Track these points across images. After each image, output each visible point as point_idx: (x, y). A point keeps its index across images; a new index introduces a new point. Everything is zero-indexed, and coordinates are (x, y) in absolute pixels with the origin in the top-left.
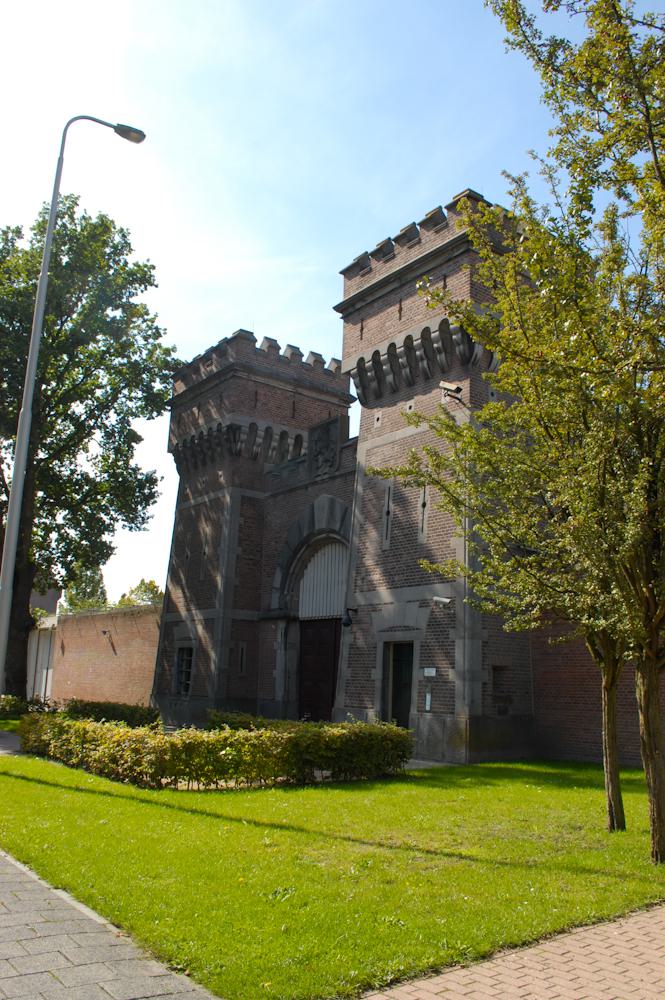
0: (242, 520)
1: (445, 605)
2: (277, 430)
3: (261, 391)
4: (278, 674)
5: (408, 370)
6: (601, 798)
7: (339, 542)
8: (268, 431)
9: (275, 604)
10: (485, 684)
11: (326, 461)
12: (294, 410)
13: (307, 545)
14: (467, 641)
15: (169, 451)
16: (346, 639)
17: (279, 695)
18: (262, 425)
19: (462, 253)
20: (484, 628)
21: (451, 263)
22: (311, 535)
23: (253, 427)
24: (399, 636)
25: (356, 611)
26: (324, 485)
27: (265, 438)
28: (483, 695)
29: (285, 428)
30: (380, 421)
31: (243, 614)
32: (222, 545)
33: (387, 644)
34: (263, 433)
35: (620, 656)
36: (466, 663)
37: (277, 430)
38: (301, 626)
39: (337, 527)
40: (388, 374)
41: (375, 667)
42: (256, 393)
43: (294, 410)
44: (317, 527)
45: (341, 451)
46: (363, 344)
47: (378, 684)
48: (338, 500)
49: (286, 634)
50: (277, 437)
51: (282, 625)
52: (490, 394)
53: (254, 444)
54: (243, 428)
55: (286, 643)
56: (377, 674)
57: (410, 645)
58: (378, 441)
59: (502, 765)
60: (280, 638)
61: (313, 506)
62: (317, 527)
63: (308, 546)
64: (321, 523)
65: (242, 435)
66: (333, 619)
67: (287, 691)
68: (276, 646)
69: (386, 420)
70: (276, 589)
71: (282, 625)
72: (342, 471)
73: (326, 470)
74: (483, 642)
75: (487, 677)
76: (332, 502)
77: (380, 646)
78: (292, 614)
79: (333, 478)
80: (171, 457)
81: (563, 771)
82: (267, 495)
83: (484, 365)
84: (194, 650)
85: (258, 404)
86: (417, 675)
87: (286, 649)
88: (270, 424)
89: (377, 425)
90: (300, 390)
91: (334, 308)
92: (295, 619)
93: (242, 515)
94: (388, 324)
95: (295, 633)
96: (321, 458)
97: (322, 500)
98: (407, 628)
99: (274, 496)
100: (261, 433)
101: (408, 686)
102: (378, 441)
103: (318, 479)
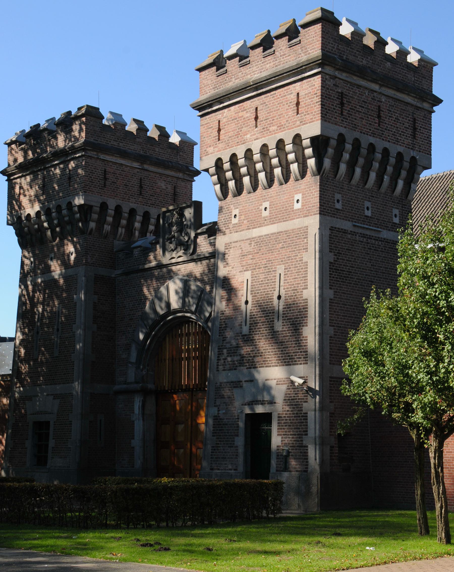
4: (137, 442)
6: (418, 167)
10: (332, 447)
14: (317, 412)
17: (138, 463)
18: (112, 204)
20: (331, 402)
27: (114, 217)
28: (331, 456)
30: (237, 217)
35: (49, 167)
36: (317, 431)
41: (237, 436)
42: (105, 171)
46: (221, 145)
49: (143, 406)
50: (126, 215)
52: (336, 201)
53: (104, 223)
54: (94, 208)
55: (143, 414)
57: (48, 423)
65: (105, 226)
69: (243, 217)
74: (330, 413)
80: (11, 230)
82: (119, 272)
84: (52, 423)
85: (108, 183)
87: (143, 420)
88: (120, 202)
89: (235, 221)
90: (146, 166)
91: (191, 105)
94: (244, 129)
100: (111, 212)
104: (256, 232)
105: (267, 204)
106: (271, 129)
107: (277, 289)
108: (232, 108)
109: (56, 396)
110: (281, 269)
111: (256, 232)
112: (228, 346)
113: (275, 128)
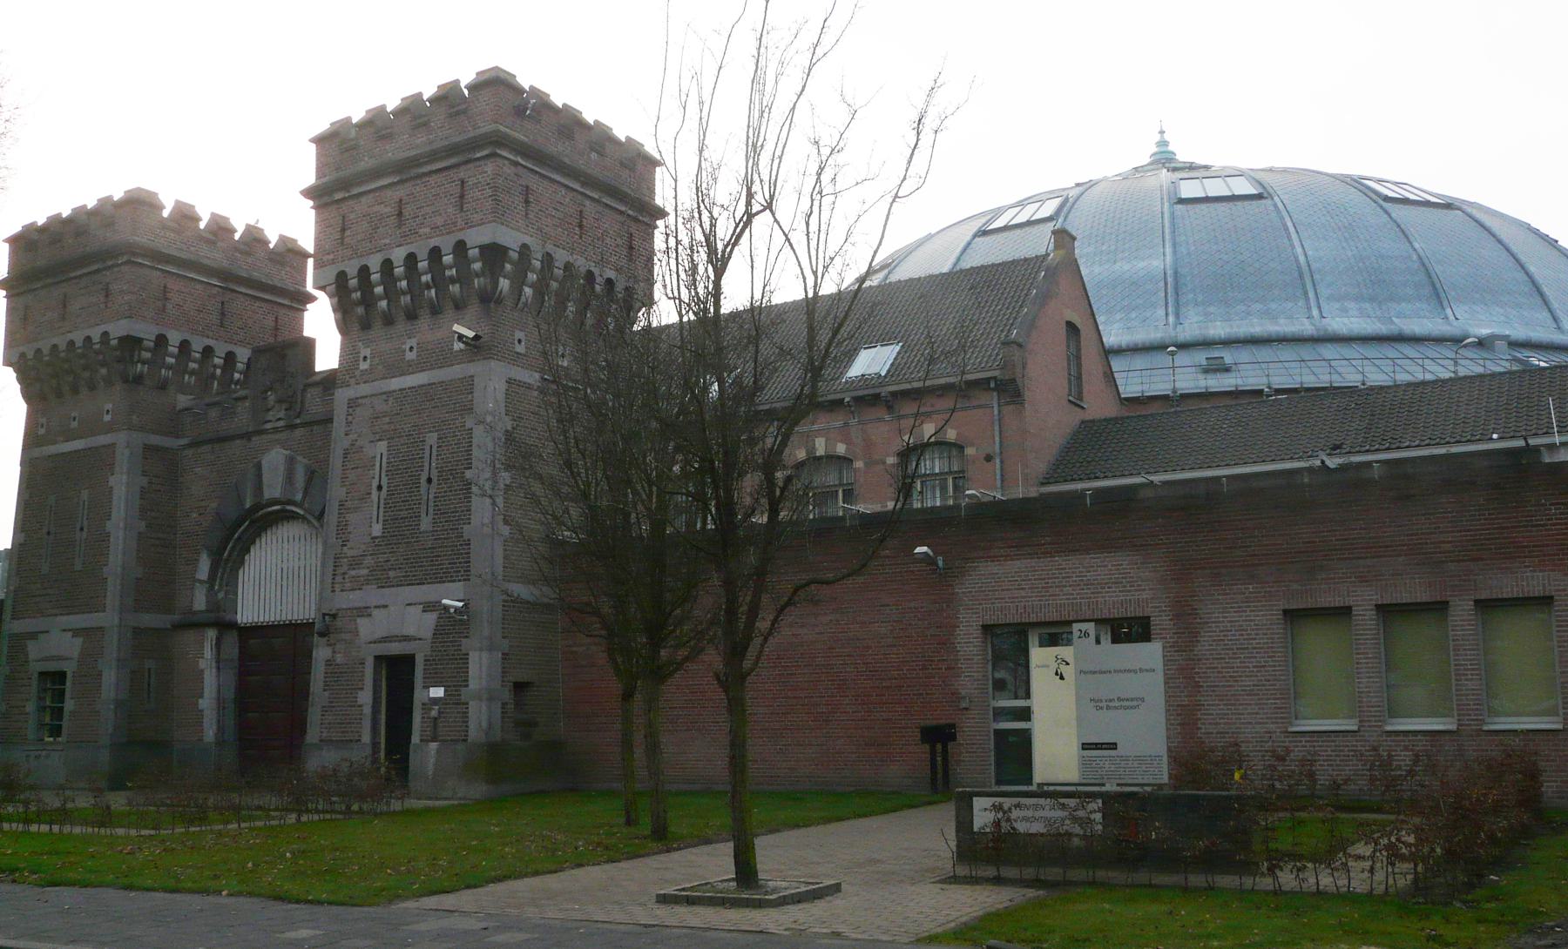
0: (144, 481)
1: (456, 609)
2: (197, 345)
3: (172, 284)
4: (207, 703)
5: (408, 298)
7: (304, 518)
8: (184, 346)
9: (200, 602)
10: (504, 705)
11: (280, 401)
12: (223, 314)
13: (248, 524)
15: (7, 363)
16: (321, 653)
17: (210, 734)
18: (174, 338)
19: (487, 156)
21: (470, 166)
22: (257, 507)
23: (161, 340)
24: (395, 649)
25: (334, 616)
26: (277, 436)
29: (211, 342)
31: (149, 620)
32: (114, 515)
33: (378, 659)
34: (176, 350)
37: (197, 345)
38: (240, 636)
39: (299, 497)
40: (381, 299)
43: (223, 314)
44: (267, 495)
45: (304, 390)
47: (367, 710)
48: (299, 458)
51: (211, 634)
56: (365, 697)
58: (365, 389)
59: (1456, 449)
60: (208, 653)
61: (259, 467)
62: (267, 495)
63: (252, 522)
64: (273, 488)
66: (291, 624)
67: (221, 729)
68: (202, 664)
70: (201, 582)
71: (211, 634)
72: (305, 418)
73: (282, 414)
75: (507, 695)
76: (291, 461)
77: (370, 662)
78: (228, 617)
79: (292, 427)
80: (10, 374)
81: (1110, 874)
82: (183, 442)
83: (509, 303)
84: (69, 675)
86: (419, 696)
92: (233, 625)
93: (144, 474)
95: (231, 640)
96: (271, 397)
97: (274, 460)
98: (407, 639)
99: (194, 444)
100: (173, 350)
101: (409, 712)
102: (365, 389)
103: (268, 426)
104: (396, 383)
105: (413, 342)
106: (421, 231)
107: (426, 468)
108: (363, 199)
109: (76, 632)
110: (432, 439)
111: (396, 383)
112: (350, 553)
113: (427, 230)
